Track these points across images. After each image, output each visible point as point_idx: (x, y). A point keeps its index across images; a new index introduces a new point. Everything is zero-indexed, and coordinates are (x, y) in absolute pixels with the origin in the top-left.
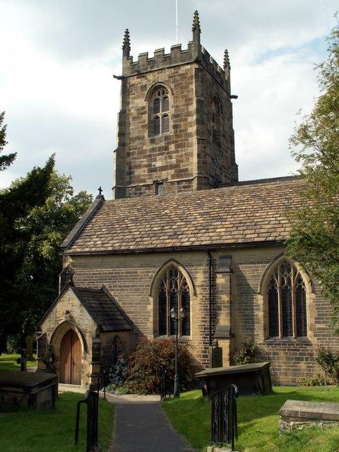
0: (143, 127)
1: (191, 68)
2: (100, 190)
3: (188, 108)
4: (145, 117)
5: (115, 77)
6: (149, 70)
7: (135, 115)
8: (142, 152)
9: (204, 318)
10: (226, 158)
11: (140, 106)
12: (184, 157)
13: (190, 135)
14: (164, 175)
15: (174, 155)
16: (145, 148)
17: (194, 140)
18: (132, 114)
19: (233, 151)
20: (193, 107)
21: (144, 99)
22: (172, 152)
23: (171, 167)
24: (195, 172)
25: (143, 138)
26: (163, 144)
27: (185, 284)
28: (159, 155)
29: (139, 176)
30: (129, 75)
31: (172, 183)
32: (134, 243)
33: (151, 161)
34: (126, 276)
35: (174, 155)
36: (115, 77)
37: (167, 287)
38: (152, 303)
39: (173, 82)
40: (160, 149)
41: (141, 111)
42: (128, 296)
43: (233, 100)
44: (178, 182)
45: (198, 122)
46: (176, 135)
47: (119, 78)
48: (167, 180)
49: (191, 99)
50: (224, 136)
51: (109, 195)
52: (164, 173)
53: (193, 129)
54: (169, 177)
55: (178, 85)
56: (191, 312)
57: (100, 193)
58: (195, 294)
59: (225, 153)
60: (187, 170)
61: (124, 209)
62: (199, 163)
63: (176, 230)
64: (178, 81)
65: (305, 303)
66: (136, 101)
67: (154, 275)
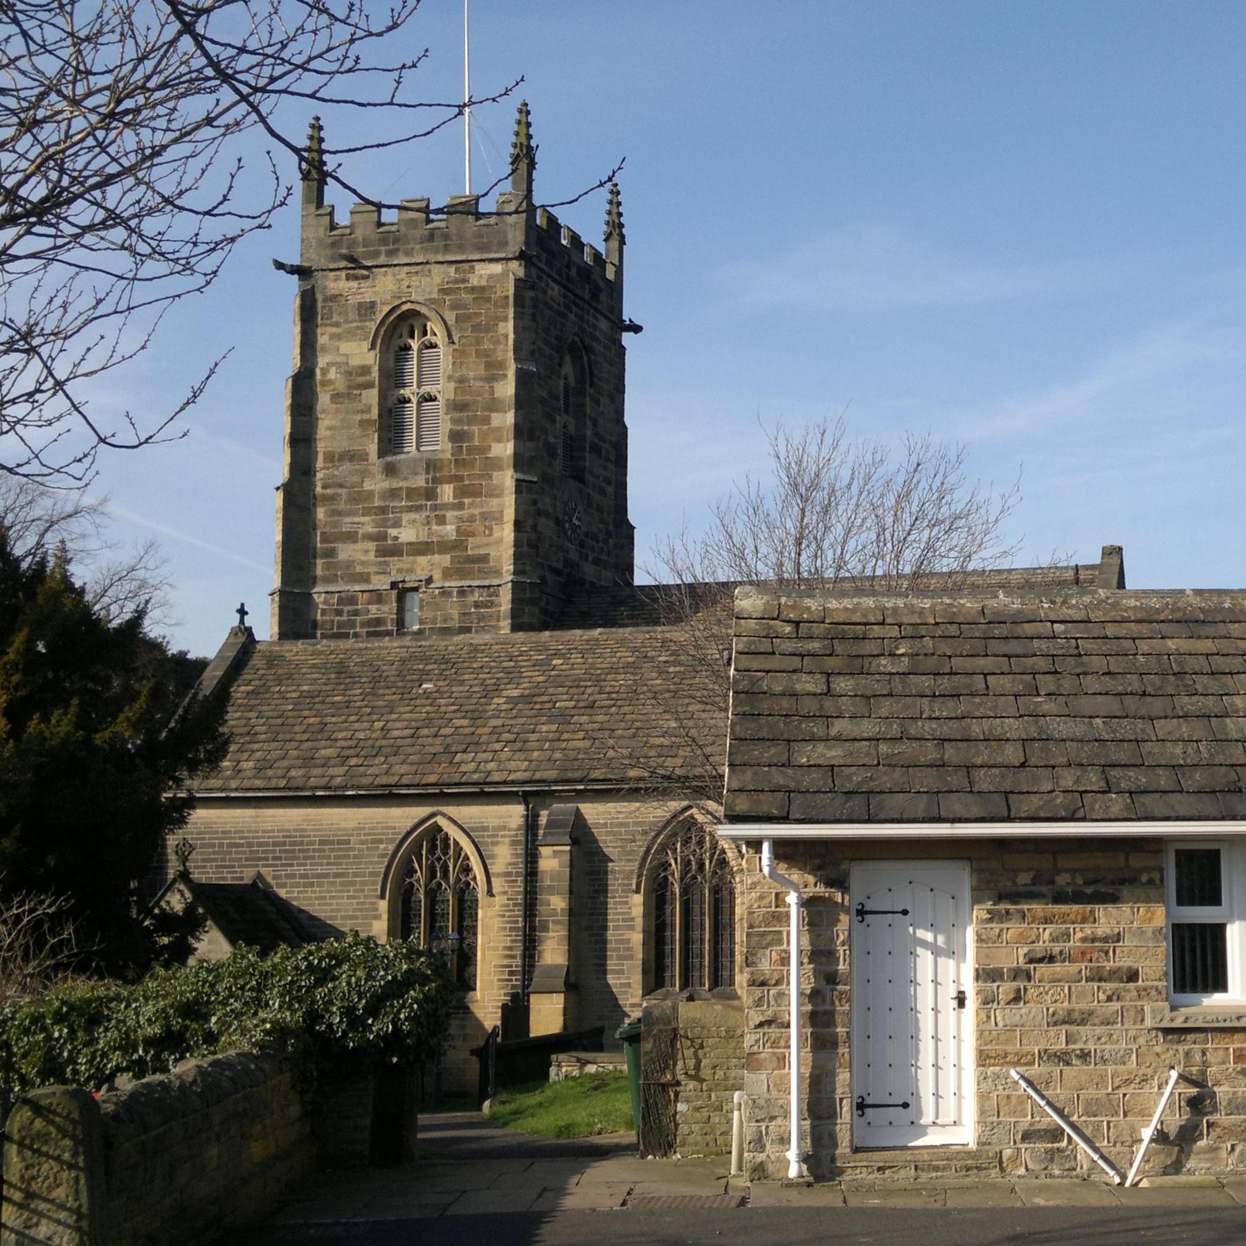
0: (363, 424)
1: (505, 274)
2: (242, 612)
3: (492, 387)
4: (371, 397)
5: (280, 266)
6: (382, 260)
7: (341, 386)
8: (359, 497)
9: (510, 948)
10: (600, 509)
11: (355, 362)
12: (478, 526)
13: (495, 464)
14: (424, 566)
15: (450, 515)
16: (368, 486)
17: (507, 479)
18: (330, 382)
19: (623, 485)
20: (507, 388)
21: (366, 345)
22: (445, 506)
23: (444, 547)
24: (508, 567)
25: (364, 457)
26: (420, 481)
27: (467, 869)
28: (410, 509)
29: (349, 564)
30: (324, 263)
31: (445, 593)
32: (341, 770)
33: (384, 524)
34: (319, 850)
35: (450, 515)
36: (280, 266)
37: (420, 875)
38: (385, 916)
39: (453, 307)
40: (411, 493)
41: (356, 377)
42: (325, 898)
43: (627, 338)
44: (462, 592)
45: (521, 432)
46: (456, 460)
47: (294, 270)
48: (429, 580)
49: (501, 365)
50: (596, 449)
51: (265, 627)
52: (422, 560)
53: (505, 449)
54: (437, 575)
55: (468, 318)
56: (479, 937)
57: (242, 621)
58: (490, 893)
59: (596, 497)
60: (484, 559)
61: (295, 650)
62: (517, 544)
63: (449, 740)
64: (465, 307)
65: (732, 913)
66: (346, 347)
67: (391, 847)
